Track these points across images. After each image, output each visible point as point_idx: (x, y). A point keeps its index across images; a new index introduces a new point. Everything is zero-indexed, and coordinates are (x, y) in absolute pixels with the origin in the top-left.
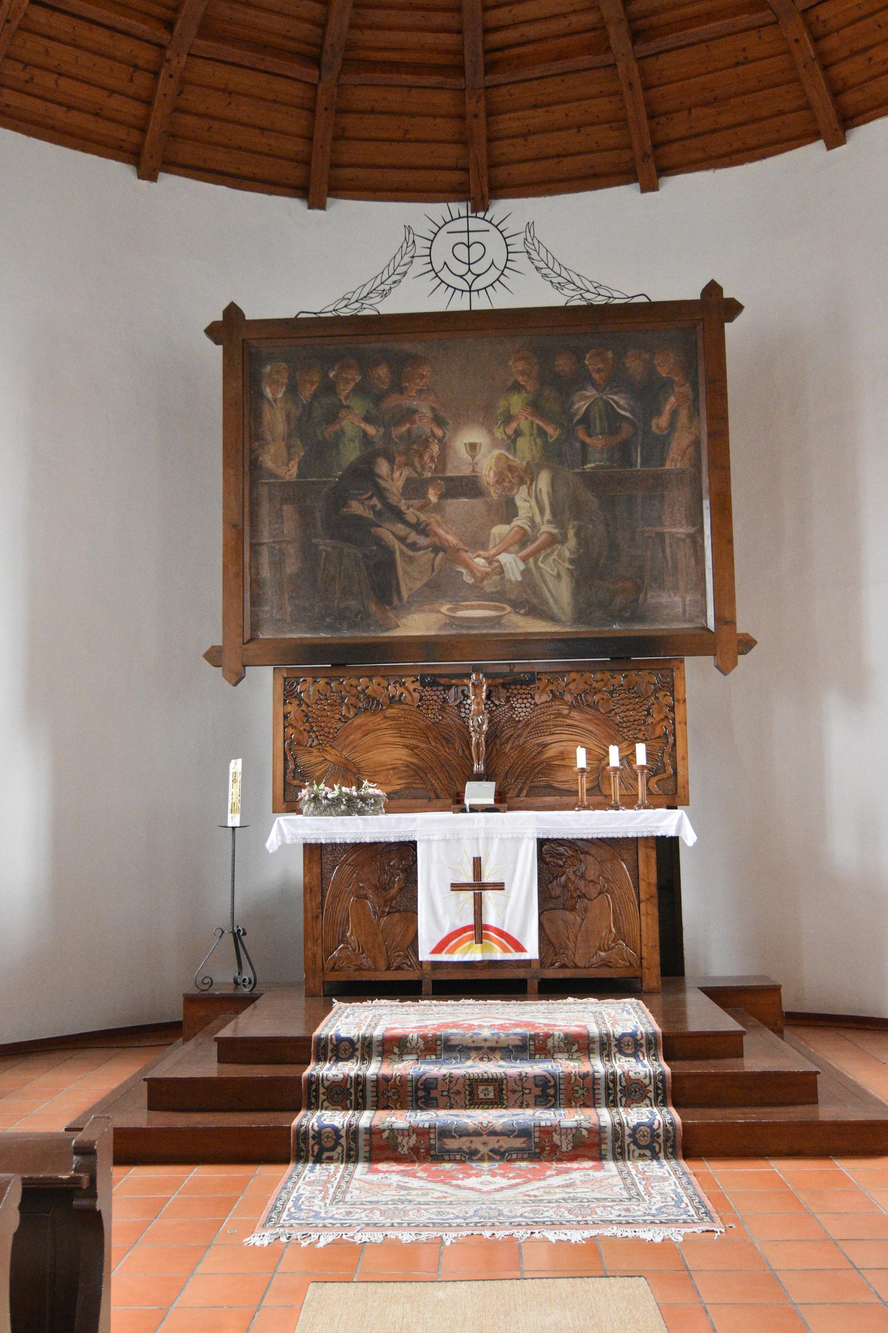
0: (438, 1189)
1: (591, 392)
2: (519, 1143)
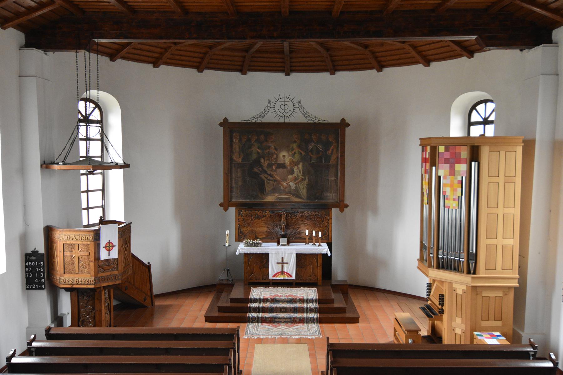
0: (274, 329)
1: (313, 144)
2: (289, 320)
